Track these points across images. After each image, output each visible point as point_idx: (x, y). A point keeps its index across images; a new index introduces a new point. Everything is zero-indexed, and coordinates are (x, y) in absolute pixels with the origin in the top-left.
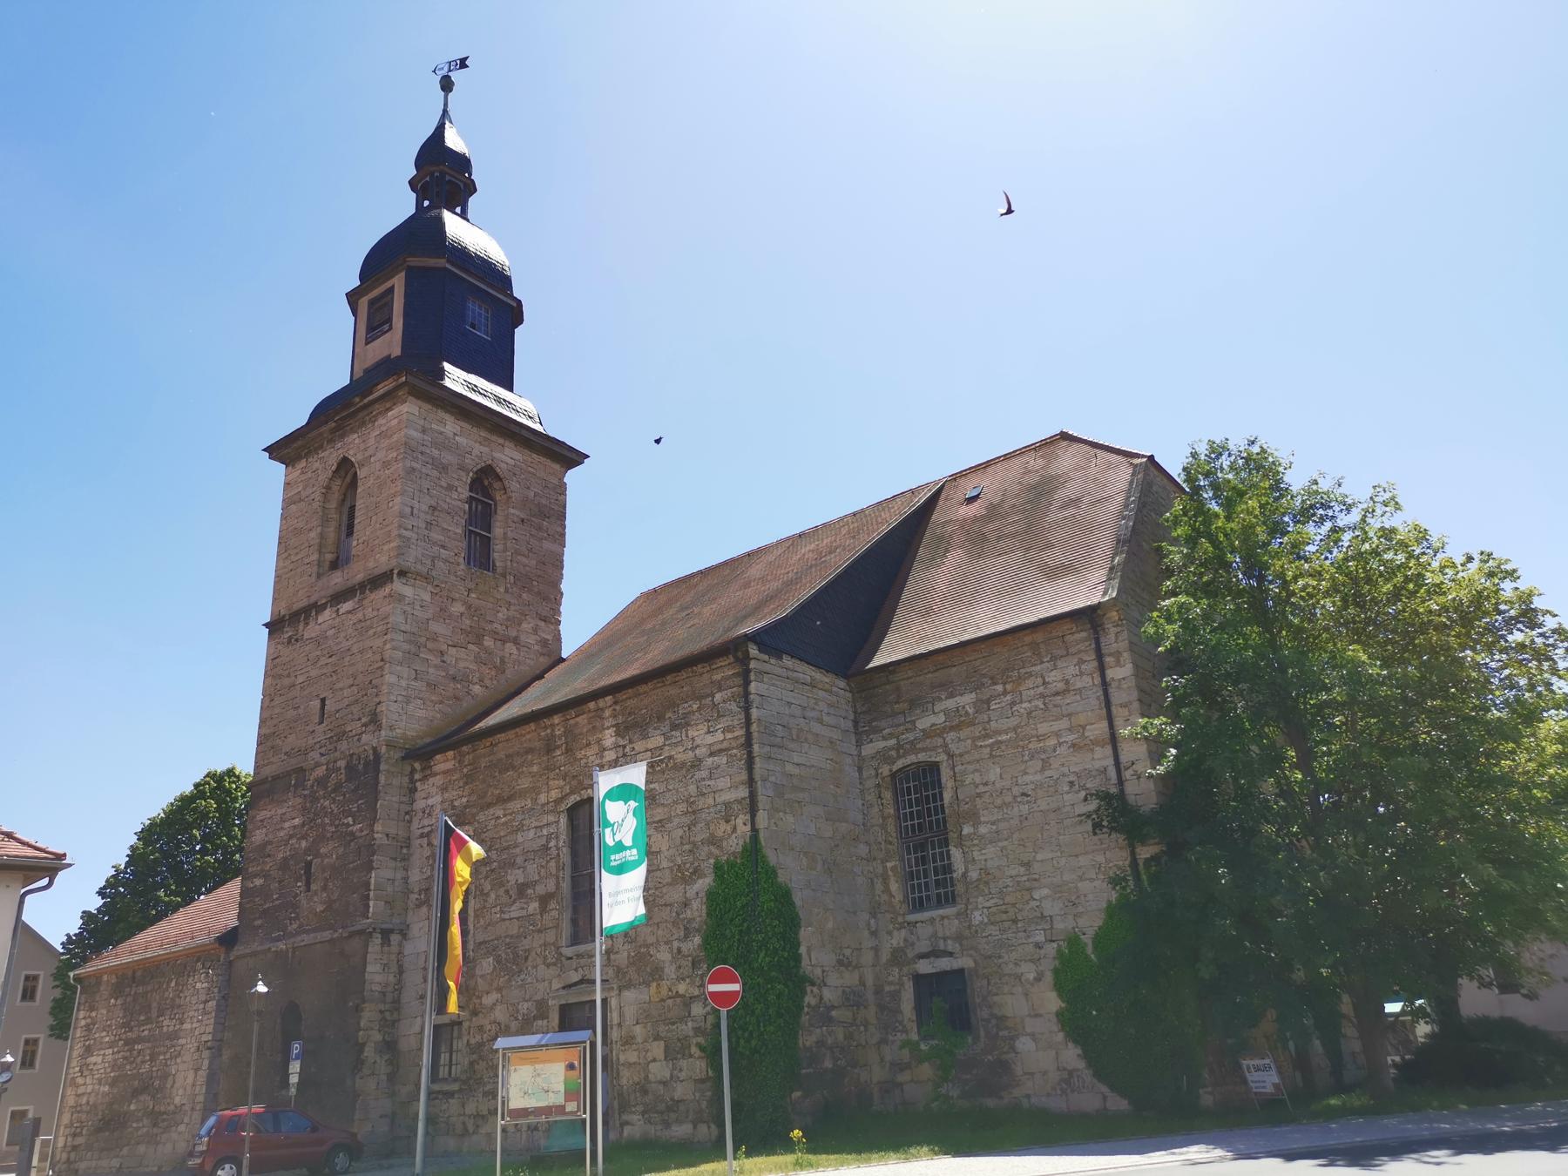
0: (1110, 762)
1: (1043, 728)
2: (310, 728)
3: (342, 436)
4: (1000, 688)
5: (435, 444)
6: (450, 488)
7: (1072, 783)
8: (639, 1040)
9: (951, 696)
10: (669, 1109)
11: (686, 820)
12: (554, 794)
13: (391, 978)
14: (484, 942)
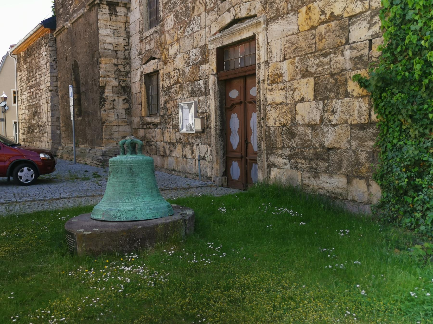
8: (286, 77)
10: (318, 157)
13: (121, 41)
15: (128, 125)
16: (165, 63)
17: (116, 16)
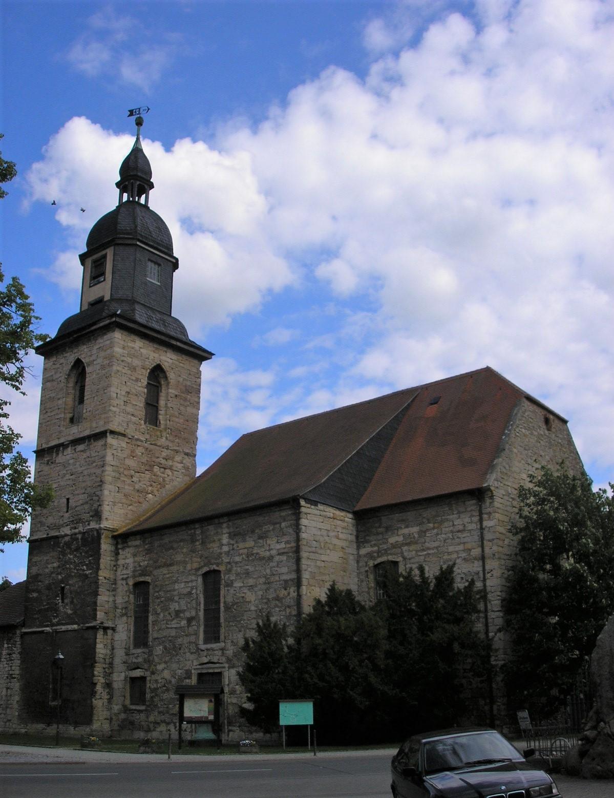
0: (480, 569)
1: (451, 549)
2: (61, 514)
3: (77, 346)
4: (431, 525)
5: (129, 355)
6: (137, 380)
7: (462, 578)
8: (238, 692)
9: (407, 527)
11: (264, 587)
12: (196, 565)
14: (158, 638)
15: (108, 710)
16: (153, 673)
17: (107, 635)
